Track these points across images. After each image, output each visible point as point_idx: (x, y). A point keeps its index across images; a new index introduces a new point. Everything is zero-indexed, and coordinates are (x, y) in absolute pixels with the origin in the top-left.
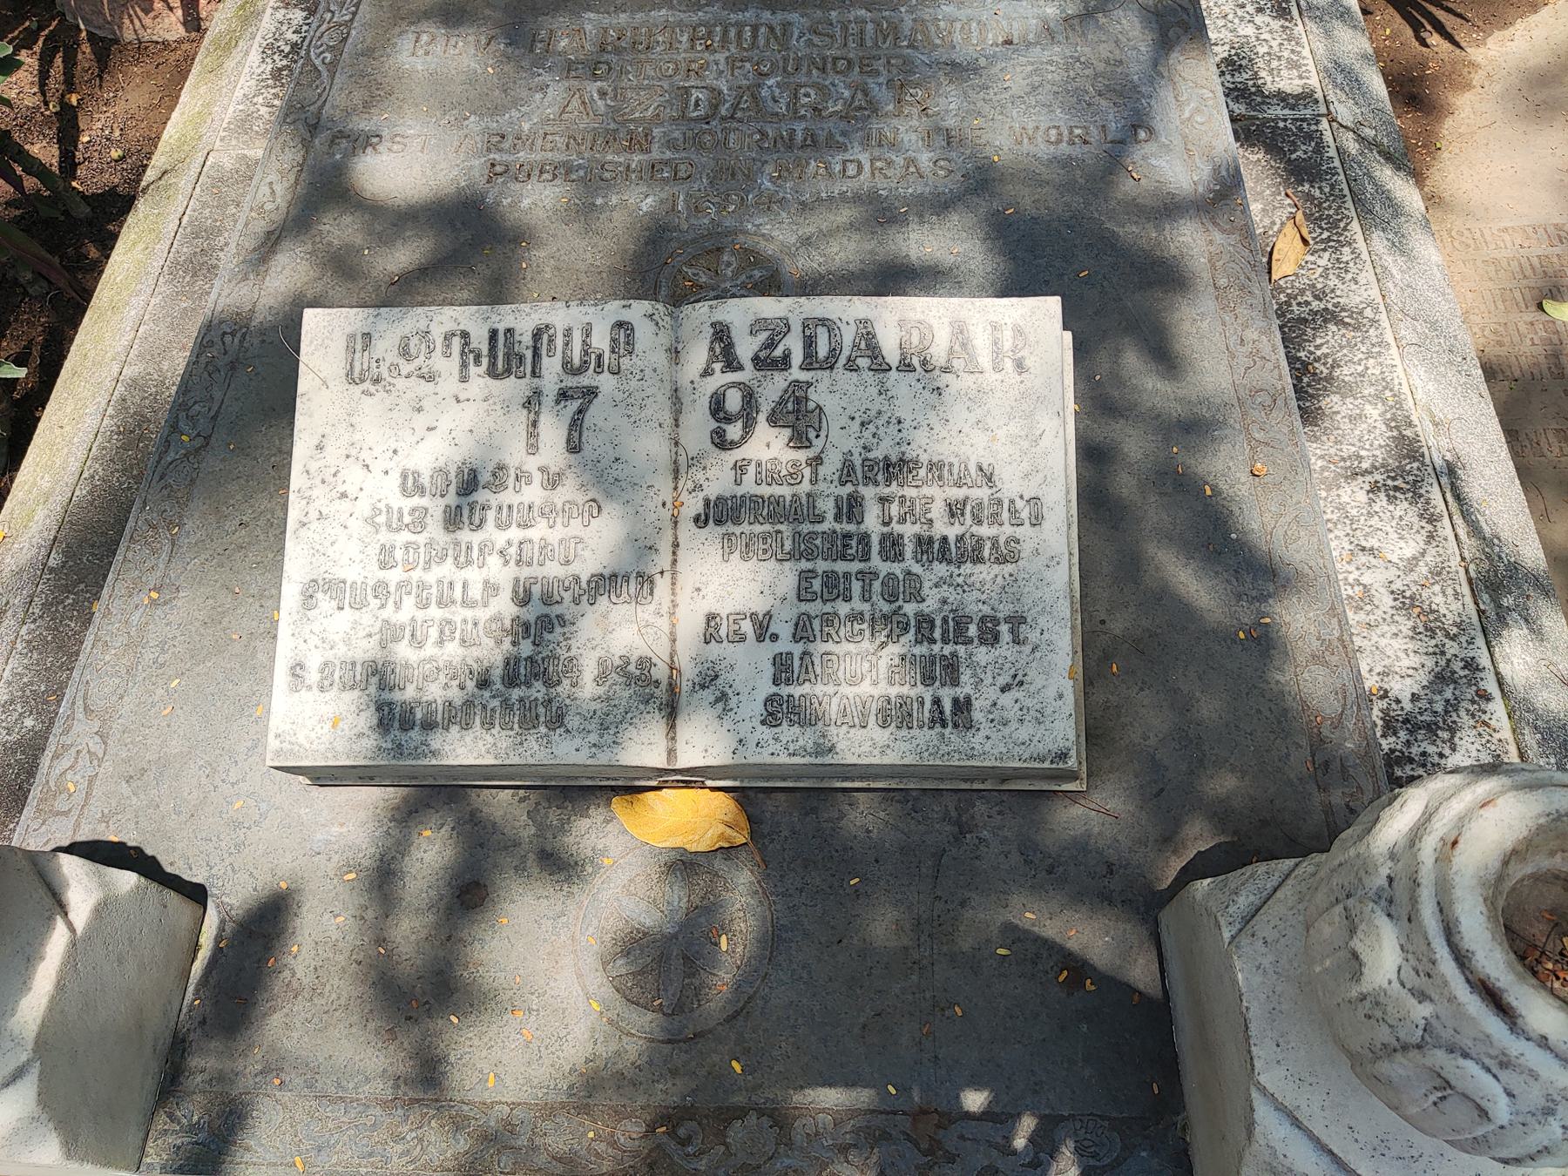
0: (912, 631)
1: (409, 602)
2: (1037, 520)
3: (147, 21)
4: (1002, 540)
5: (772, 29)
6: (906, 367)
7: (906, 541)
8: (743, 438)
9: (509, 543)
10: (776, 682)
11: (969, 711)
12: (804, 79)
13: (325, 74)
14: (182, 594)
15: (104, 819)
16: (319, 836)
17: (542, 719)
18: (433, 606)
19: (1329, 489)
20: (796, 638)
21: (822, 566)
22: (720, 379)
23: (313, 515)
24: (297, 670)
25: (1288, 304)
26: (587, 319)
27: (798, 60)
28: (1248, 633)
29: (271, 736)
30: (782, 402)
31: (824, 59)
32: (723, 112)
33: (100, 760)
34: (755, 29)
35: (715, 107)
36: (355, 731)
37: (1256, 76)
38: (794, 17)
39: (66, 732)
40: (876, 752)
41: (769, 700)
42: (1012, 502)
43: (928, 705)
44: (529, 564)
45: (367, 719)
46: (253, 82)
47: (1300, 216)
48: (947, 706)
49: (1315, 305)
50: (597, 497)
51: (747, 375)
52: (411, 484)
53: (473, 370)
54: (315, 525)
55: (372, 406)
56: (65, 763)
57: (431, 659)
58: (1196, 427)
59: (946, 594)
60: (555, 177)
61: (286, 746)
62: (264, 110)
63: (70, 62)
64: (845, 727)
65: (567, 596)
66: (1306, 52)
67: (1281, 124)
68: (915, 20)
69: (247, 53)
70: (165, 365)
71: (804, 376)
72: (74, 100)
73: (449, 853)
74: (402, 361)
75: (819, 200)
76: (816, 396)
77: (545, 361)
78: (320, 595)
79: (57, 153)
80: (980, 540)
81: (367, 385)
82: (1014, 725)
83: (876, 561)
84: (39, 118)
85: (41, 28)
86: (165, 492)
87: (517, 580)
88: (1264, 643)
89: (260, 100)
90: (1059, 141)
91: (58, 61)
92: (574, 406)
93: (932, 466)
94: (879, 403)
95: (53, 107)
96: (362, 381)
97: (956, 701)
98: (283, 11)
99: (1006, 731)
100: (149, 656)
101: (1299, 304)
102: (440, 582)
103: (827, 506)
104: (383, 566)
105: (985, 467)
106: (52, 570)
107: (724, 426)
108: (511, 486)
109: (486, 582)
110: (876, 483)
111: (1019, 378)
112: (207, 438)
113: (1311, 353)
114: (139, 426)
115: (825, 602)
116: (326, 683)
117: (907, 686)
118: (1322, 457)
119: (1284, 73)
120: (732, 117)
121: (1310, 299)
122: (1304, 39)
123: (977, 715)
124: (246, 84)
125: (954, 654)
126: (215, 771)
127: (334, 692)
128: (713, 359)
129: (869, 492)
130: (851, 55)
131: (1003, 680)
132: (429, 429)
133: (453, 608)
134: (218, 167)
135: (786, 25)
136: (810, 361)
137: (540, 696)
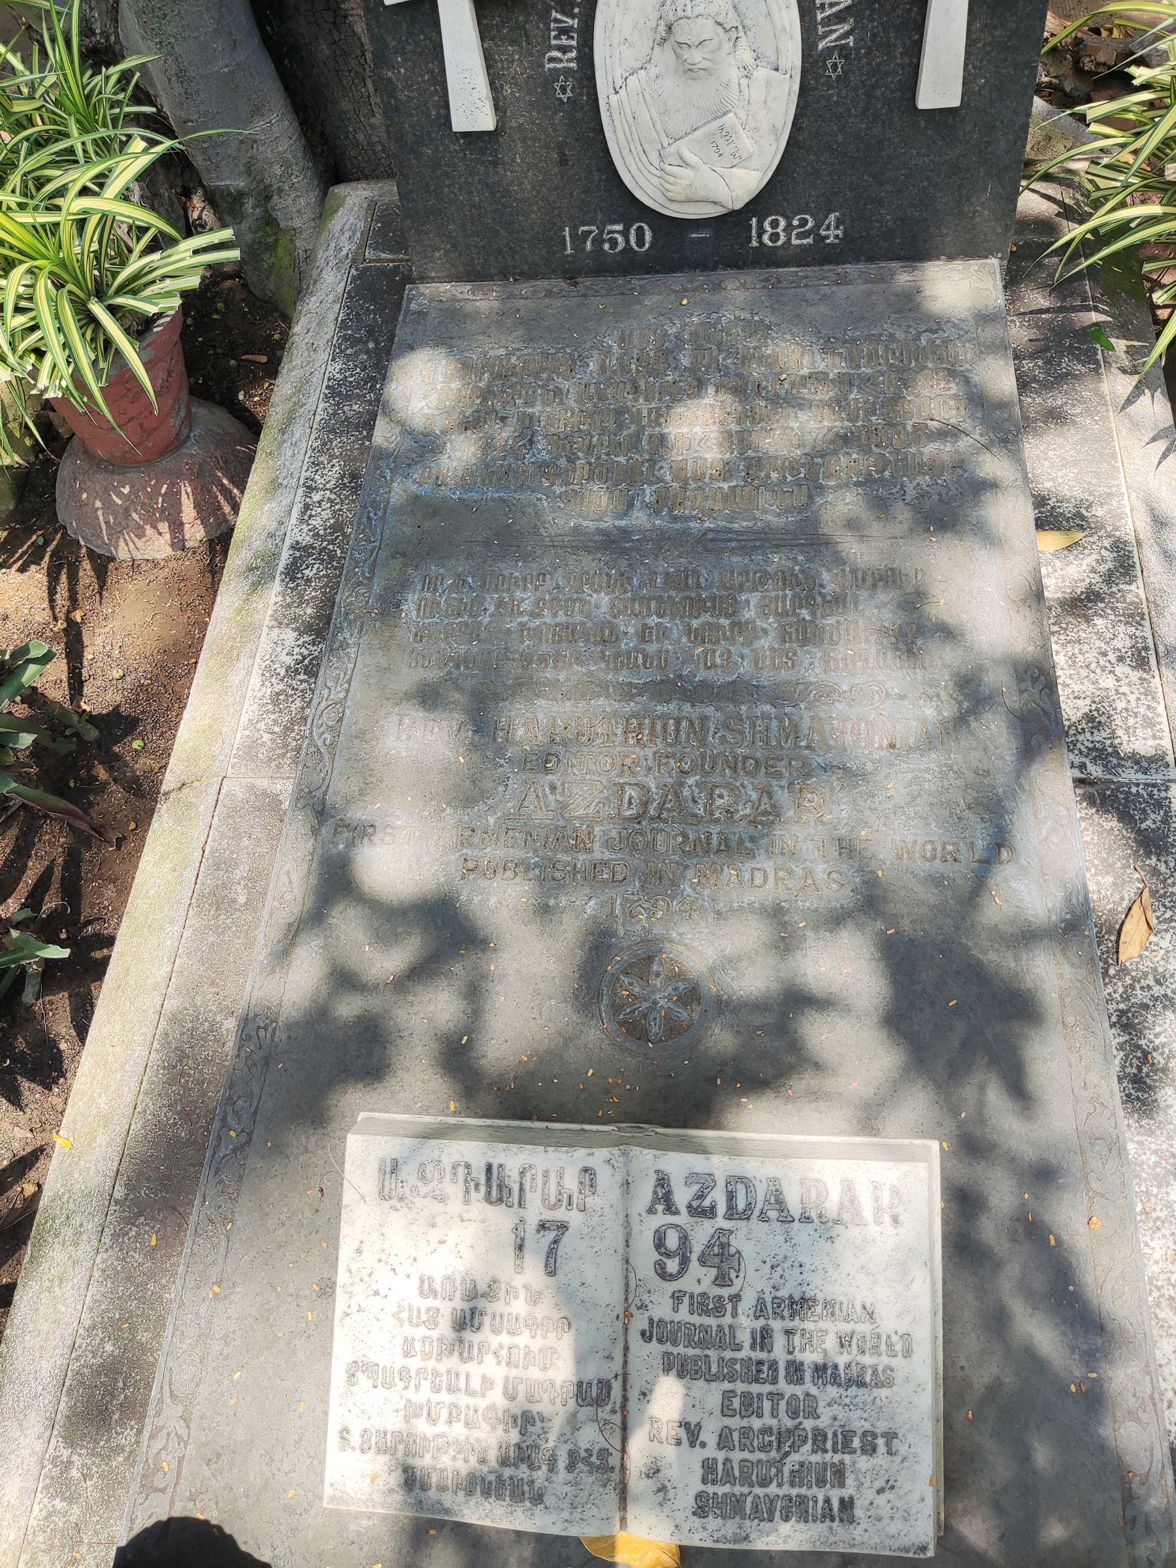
0: (810, 1442)
1: (426, 1386)
2: (908, 1353)
3: (140, 544)
4: (880, 1369)
5: (692, 723)
6: (806, 1219)
7: (806, 1368)
8: (679, 1272)
9: (501, 1346)
10: (704, 1481)
11: (852, 1508)
12: (718, 779)
13: (326, 757)
14: (238, 1290)
15: (192, 1498)
16: (352, 1527)
17: (527, 1496)
18: (444, 1391)
19: (1159, 1186)
20: (720, 1446)
21: (740, 1387)
22: (661, 1219)
23: (354, 1308)
24: (344, 1434)
25: (1133, 987)
26: (560, 1164)
27: (714, 758)
28: (1079, 1386)
29: (327, 1485)
30: (709, 1246)
31: (735, 758)
32: (652, 812)
33: (186, 1443)
34: (678, 722)
35: (645, 804)
36: (387, 1487)
37: (1113, 736)
38: (710, 710)
39: (158, 1414)
40: (780, 1541)
41: (699, 1496)
42: (889, 1337)
43: (820, 1503)
44: (517, 1367)
45: (395, 1479)
46: (255, 707)
47: (1146, 894)
48: (835, 1504)
49: (1157, 990)
50: (569, 1316)
51: (683, 1219)
52: (427, 1288)
53: (474, 1195)
54: (355, 1316)
55: (397, 1221)
56: (159, 1444)
57: (443, 1435)
58: (1043, 1175)
59: (837, 1412)
60: (516, 874)
61: (338, 1494)
62: (266, 737)
63: (73, 579)
64: (756, 1521)
65: (545, 1397)
66: (1161, 709)
67: (1134, 790)
68: (812, 718)
69: (249, 673)
70: (199, 1000)
71: (727, 1225)
72: (77, 616)
73: (450, 1550)
74: (420, 1184)
75: (731, 909)
76: (737, 1243)
77: (528, 1194)
78: (359, 1374)
79: (65, 668)
80: (863, 1368)
81: (394, 1202)
82: (886, 1521)
83: (782, 1385)
84: (48, 633)
85: (47, 543)
86: (220, 1187)
87: (507, 1378)
88: (1093, 1399)
89: (262, 725)
90: (934, 857)
91: (64, 578)
92: (550, 1236)
93: (826, 1304)
94: (785, 1249)
95: (61, 625)
96: (390, 1198)
97: (842, 1500)
98: (277, 631)
99: (880, 1526)
100: (216, 1347)
101: (1142, 988)
102: (449, 1371)
103: (744, 1337)
104: (406, 1354)
105: (868, 1306)
106: (117, 1202)
107: (665, 1260)
108: (502, 1297)
109: (484, 1377)
110: (783, 1318)
111: (894, 1231)
112: (250, 1134)
113: (1151, 1042)
114: (180, 1061)
115: (742, 1417)
116: (366, 1446)
117: (805, 1488)
118: (1155, 1152)
119: (1140, 732)
120: (659, 817)
121: (1152, 983)
122: (1160, 694)
123: (858, 1512)
124: (250, 709)
125: (842, 1463)
126: (273, 1460)
127: (370, 1455)
128: (656, 1200)
129: (777, 1325)
130: (758, 755)
131: (879, 1484)
132: (441, 1242)
133: (459, 1395)
134: (231, 796)
135: (704, 719)
136: (732, 1213)
137: (525, 1476)
